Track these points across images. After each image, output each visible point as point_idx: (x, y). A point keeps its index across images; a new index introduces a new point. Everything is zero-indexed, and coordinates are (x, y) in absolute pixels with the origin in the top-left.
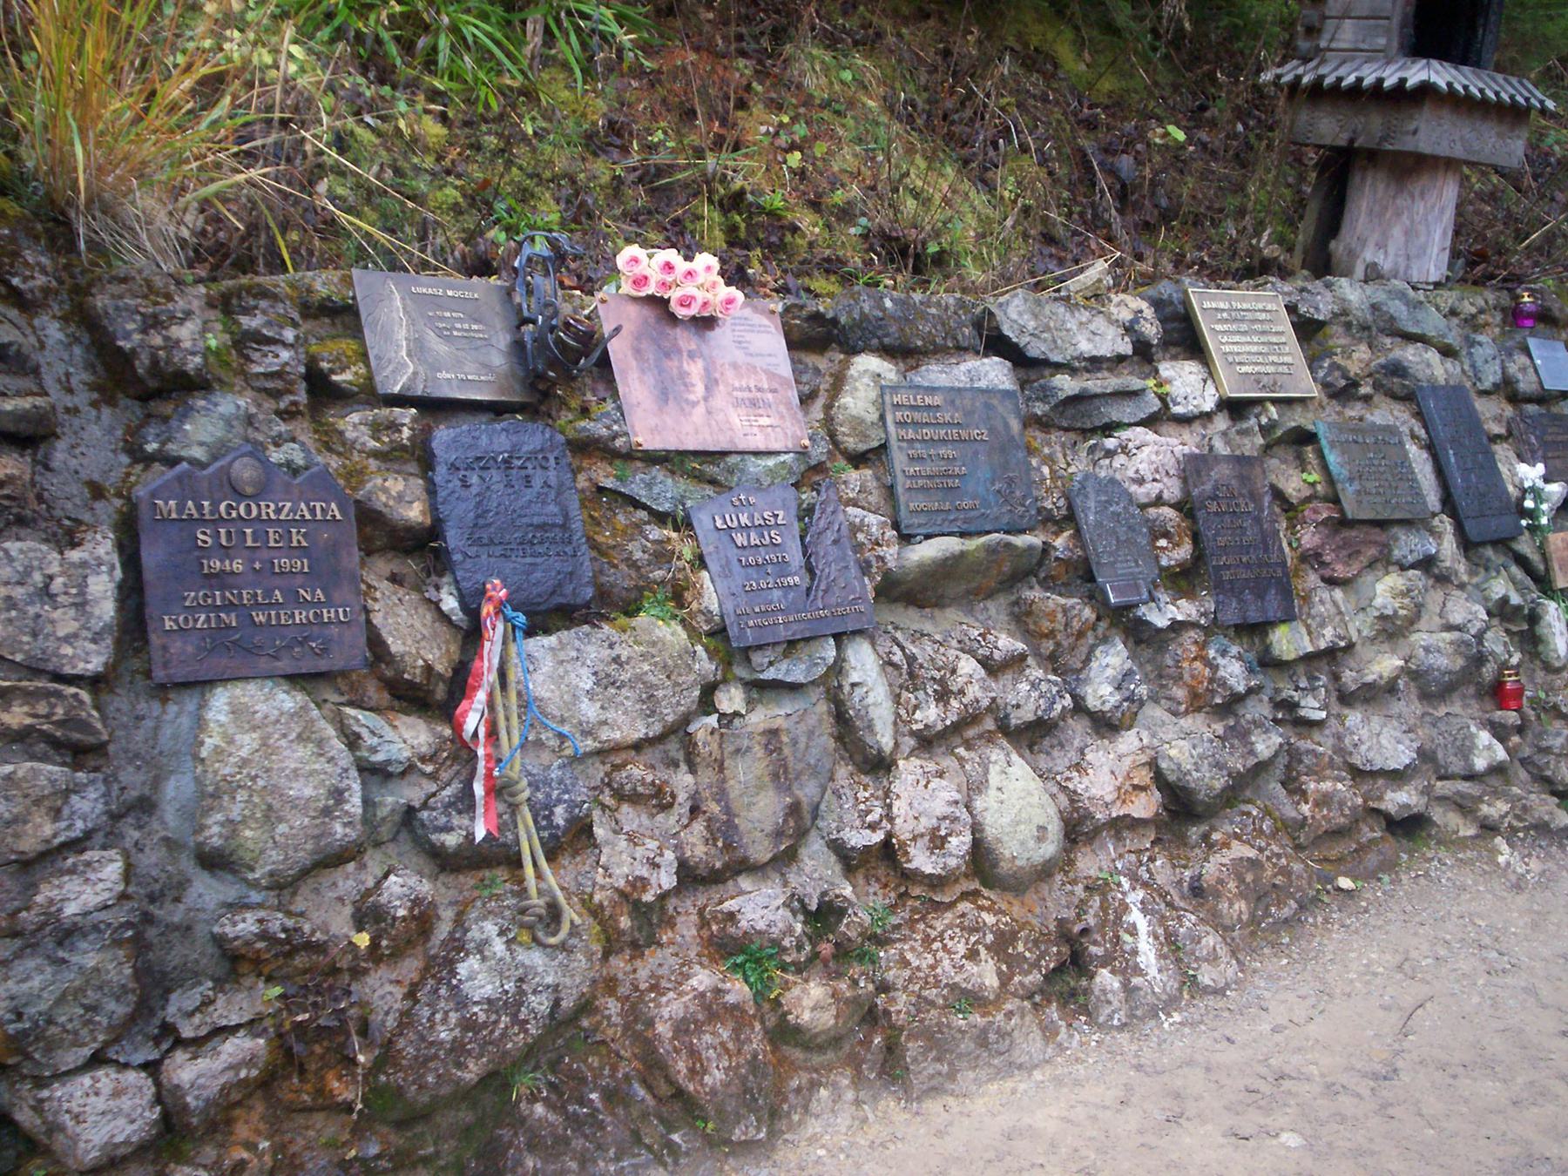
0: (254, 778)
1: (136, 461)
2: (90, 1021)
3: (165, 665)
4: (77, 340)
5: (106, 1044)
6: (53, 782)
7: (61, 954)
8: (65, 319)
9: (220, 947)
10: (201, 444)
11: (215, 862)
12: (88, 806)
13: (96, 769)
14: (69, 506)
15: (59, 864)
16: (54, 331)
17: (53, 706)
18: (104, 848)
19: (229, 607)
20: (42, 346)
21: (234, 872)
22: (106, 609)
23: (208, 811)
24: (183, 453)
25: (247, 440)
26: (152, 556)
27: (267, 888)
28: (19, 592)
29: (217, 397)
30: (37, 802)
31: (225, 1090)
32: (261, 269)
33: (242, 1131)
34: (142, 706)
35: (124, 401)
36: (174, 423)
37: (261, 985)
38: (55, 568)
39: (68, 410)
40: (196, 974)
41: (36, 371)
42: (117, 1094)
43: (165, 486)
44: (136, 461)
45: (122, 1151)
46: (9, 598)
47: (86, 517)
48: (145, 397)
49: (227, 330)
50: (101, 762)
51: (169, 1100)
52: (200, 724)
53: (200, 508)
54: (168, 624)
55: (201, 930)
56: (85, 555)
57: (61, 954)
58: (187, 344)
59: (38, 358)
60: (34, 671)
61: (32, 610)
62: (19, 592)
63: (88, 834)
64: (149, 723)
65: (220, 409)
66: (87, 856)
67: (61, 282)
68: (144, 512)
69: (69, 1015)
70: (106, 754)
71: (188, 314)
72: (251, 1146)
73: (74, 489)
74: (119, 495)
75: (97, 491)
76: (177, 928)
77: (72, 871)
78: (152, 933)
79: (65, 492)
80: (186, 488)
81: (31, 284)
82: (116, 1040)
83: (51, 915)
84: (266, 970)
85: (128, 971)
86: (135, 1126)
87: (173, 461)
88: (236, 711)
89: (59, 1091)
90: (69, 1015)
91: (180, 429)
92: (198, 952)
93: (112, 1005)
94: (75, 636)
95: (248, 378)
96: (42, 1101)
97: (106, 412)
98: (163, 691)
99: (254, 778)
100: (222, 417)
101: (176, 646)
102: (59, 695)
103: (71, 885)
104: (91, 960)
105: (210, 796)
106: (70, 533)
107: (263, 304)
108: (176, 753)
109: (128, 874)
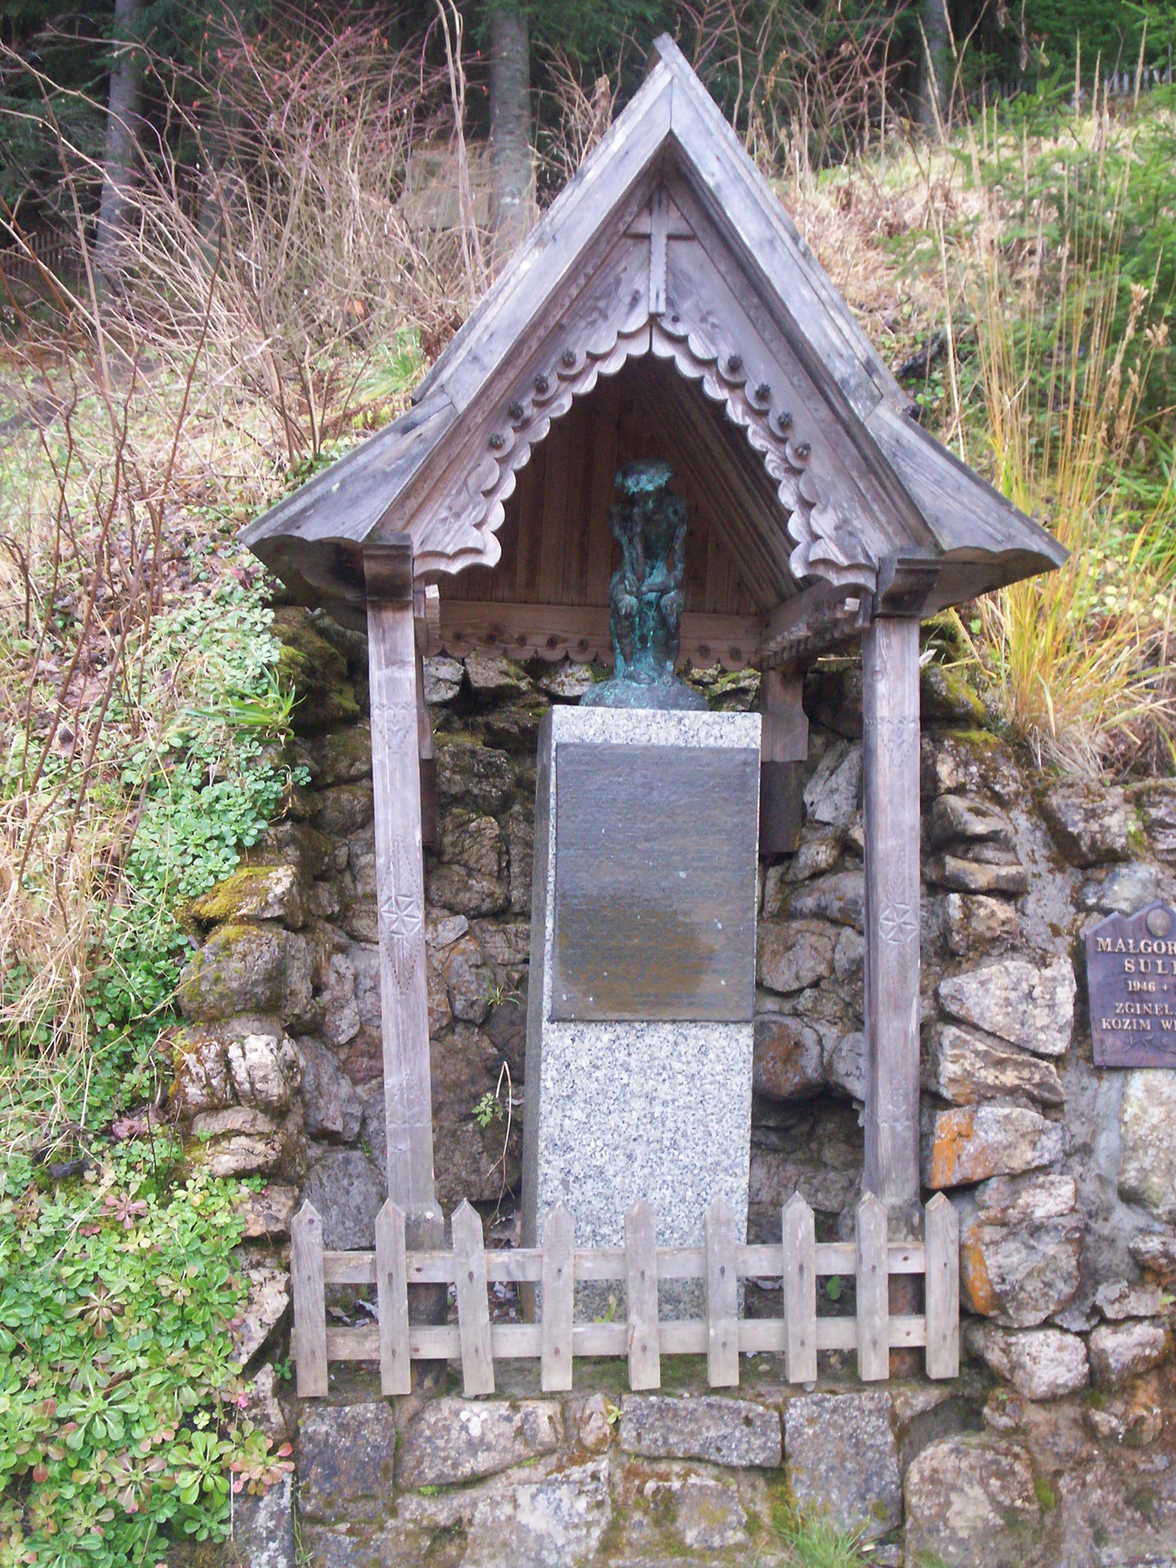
0: (1161, 1140)
1: (1079, 910)
2: (1045, 1294)
3: (1102, 1053)
4: (1038, 827)
5: (1055, 1313)
6: (1034, 1124)
7: (1032, 1242)
8: (1029, 813)
9: (1134, 1258)
10: (1126, 899)
11: (1131, 1197)
12: (1051, 1145)
13: (1056, 1120)
14: (1039, 940)
15: (1034, 1180)
16: (1023, 822)
17: (1032, 1073)
18: (1062, 1174)
19: (1145, 1015)
20: (1017, 832)
21: (1144, 1207)
22: (1067, 1011)
23: (1127, 1160)
24: (1114, 906)
25: (1156, 897)
26: (1094, 976)
27: (1168, 1223)
28: (1013, 995)
29: (1135, 866)
30: (1023, 1136)
31: (1136, 1360)
32: (1155, 771)
33: (1142, 1396)
34: (1085, 1081)
35: (1070, 869)
36: (1106, 884)
37: (1160, 1292)
38: (1035, 981)
39: (1034, 875)
40: (1117, 1275)
41: (1013, 849)
42: (1061, 1348)
43: (1103, 928)
44: (1079, 910)
45: (1061, 1391)
46: (1007, 999)
47: (1050, 948)
48: (1085, 866)
49: (1139, 818)
50: (1059, 1116)
51: (1095, 1361)
52: (1123, 1096)
53: (1127, 944)
54: (1105, 1025)
55: (1121, 1244)
56: (1055, 973)
57: (1032, 1242)
58: (1115, 830)
59: (1015, 840)
60: (1021, 1049)
61: (1021, 1008)
62: (1013, 995)
63: (1052, 1163)
64: (1089, 1093)
65: (1139, 875)
66: (1052, 1177)
67: (1025, 787)
68: (1089, 945)
69: (1033, 1286)
70: (1062, 1111)
71: (1115, 808)
72: (1149, 1409)
73: (1042, 929)
74: (1070, 933)
75: (1056, 931)
76: (1106, 1239)
77: (1041, 1186)
78: (1089, 1239)
79: (1036, 931)
80: (1117, 930)
81: (1007, 789)
82: (1062, 1311)
83: (1026, 1216)
84: (1164, 1282)
85: (1074, 1263)
86: (1071, 1375)
87: (1107, 912)
88: (1149, 1091)
89: (1022, 1339)
90: (1033, 1286)
91: (1110, 888)
92: (1119, 1259)
93: (1060, 1285)
94: (1048, 1027)
95: (1155, 853)
96: (1010, 1345)
97: (1059, 876)
98: (1100, 1071)
99: (1161, 1140)
100: (1140, 880)
101: (1109, 1040)
102: (1036, 1066)
103: (1041, 1196)
104: (1051, 1250)
105: (1129, 1150)
106: (1043, 958)
107: (1166, 799)
108: (1106, 1116)
109: (1077, 1194)
